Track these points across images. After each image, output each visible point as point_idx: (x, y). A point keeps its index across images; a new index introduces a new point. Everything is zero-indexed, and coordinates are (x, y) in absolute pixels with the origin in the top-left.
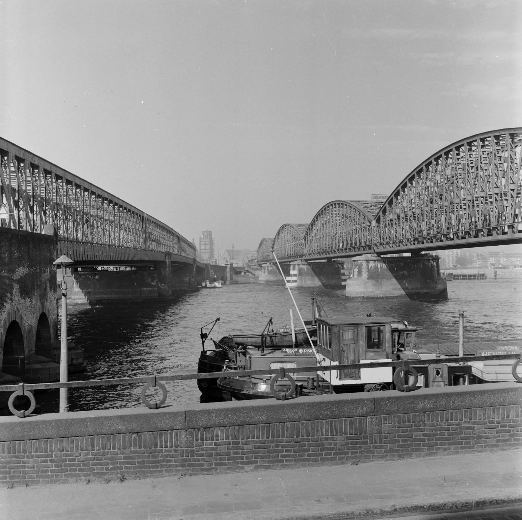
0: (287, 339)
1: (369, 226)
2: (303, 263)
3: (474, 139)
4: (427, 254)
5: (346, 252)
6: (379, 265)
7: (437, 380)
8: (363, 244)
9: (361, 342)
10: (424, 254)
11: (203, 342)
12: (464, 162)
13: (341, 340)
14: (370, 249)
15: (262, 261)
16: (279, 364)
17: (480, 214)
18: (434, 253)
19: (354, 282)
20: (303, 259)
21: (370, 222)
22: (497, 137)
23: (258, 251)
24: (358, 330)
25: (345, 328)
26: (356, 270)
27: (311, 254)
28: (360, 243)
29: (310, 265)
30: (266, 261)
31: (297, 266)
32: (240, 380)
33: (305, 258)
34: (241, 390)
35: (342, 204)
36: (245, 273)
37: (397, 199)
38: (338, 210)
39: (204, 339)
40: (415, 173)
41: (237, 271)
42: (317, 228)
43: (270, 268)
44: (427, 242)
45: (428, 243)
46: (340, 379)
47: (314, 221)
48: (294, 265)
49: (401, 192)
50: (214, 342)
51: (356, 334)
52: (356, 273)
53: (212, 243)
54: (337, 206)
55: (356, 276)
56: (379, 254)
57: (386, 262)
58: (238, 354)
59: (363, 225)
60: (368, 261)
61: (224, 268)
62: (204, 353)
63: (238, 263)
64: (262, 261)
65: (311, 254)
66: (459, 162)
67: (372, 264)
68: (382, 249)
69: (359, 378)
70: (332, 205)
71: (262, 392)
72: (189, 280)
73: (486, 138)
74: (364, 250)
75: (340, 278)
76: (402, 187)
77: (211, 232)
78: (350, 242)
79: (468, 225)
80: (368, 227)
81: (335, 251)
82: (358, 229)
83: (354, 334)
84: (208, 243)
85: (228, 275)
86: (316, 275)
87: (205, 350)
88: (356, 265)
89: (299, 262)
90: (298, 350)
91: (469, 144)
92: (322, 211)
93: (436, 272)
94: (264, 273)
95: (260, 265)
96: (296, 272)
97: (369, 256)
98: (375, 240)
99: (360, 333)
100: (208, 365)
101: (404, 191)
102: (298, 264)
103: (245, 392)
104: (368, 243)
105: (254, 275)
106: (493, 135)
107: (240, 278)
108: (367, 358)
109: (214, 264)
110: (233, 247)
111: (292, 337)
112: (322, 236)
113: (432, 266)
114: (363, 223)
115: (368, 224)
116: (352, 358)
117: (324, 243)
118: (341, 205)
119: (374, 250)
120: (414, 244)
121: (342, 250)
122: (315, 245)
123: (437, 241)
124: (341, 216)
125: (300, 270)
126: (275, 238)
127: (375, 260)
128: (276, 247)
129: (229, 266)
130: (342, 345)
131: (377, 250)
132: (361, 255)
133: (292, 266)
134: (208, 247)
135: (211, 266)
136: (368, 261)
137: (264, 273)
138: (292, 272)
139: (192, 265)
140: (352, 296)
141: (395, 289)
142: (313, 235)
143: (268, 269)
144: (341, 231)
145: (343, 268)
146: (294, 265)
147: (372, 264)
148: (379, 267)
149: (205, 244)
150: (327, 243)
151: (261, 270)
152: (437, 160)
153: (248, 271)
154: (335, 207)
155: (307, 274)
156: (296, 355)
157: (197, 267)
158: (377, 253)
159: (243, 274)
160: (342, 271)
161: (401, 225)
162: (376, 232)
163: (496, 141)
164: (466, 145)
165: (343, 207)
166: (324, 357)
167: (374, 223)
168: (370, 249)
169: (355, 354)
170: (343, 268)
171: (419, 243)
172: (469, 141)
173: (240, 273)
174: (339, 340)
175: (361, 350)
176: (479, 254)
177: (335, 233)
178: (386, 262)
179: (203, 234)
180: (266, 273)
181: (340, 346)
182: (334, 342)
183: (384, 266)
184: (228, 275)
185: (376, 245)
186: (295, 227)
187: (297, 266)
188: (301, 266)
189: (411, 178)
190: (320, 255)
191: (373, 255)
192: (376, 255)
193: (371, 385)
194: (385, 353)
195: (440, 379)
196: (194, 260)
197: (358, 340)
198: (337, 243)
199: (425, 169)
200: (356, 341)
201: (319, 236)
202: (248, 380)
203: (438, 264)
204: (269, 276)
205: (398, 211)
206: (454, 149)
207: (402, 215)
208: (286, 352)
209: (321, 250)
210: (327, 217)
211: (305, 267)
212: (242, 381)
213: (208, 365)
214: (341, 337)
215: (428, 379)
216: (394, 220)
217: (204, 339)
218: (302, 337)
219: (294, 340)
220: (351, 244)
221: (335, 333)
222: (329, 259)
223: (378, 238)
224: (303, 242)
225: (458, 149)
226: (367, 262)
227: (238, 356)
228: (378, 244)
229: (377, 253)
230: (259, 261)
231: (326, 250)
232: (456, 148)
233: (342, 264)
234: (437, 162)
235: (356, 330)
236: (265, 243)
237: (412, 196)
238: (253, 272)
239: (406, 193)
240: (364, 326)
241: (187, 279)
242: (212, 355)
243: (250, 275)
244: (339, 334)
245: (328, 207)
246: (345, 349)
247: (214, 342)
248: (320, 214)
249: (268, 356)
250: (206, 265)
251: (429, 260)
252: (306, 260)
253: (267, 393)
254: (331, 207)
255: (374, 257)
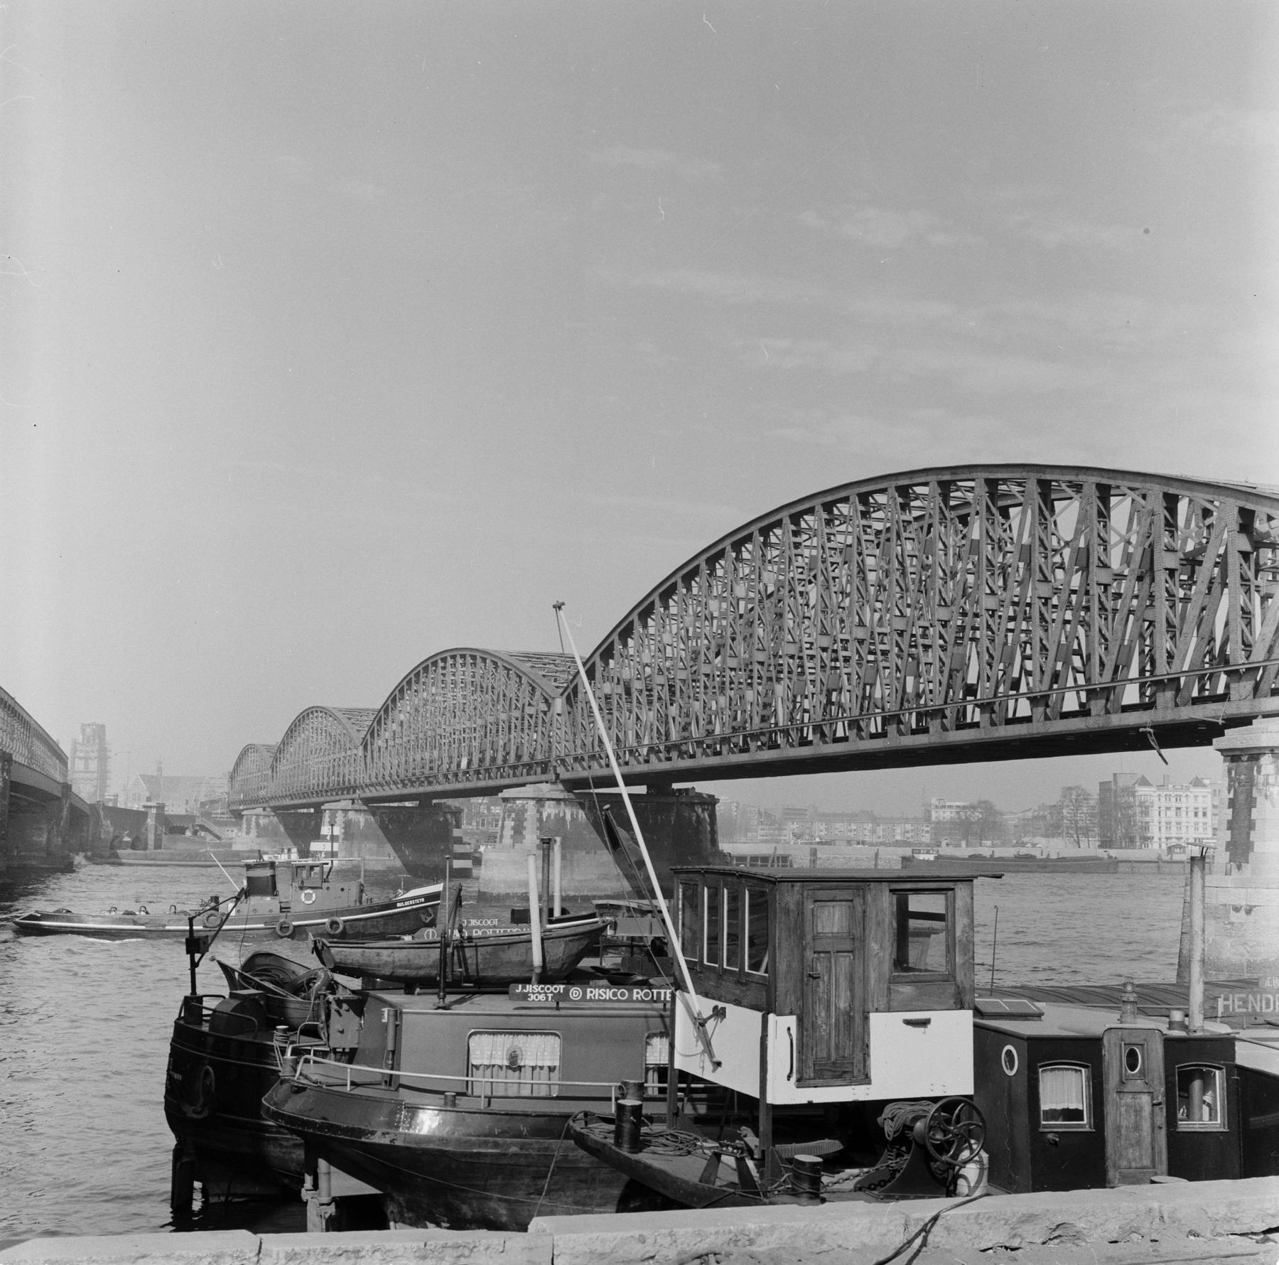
0: (513, 955)
1: (545, 713)
2: (356, 807)
3: (842, 494)
4: (687, 790)
5: (478, 779)
6: (568, 812)
7: (1130, 1087)
8: (526, 759)
9: (874, 946)
10: (679, 790)
11: (194, 965)
12: (814, 552)
13: (809, 937)
14: (544, 771)
15: (241, 802)
16: (500, 1038)
17: (854, 682)
18: (703, 787)
19: (503, 856)
20: (356, 796)
21: (546, 701)
22: (904, 491)
23: (232, 778)
24: (865, 903)
25: (822, 894)
26: (509, 824)
27: (372, 785)
28: (519, 757)
29: (374, 815)
30: (252, 802)
31: (340, 815)
32: (360, 1097)
33: (363, 795)
34: (362, 1133)
35: (474, 657)
36: (195, 833)
37: (625, 645)
38: (463, 673)
39: (197, 956)
40: (678, 578)
41: (173, 827)
42: (402, 717)
43: (262, 821)
44: (705, 753)
45: (708, 756)
46: (801, 1082)
47: (394, 701)
48: (334, 812)
49: (638, 629)
50: (224, 967)
51: (859, 914)
52: (508, 832)
53: (103, 757)
54: (460, 661)
55: (507, 840)
56: (571, 785)
57: (587, 804)
58: (334, 1006)
59: (529, 710)
60: (540, 801)
61: (140, 816)
62: (192, 1004)
63: (175, 808)
64: (241, 802)
65: (372, 785)
66: (799, 551)
67: (550, 810)
68: (580, 772)
69: (866, 1079)
70: (444, 660)
71: (428, 1139)
72: (49, 839)
73: (323, 803)
74: (528, 774)
75: (449, 851)
76: (640, 615)
77: (103, 726)
78: (489, 753)
79: (820, 711)
80: (541, 715)
81: (446, 776)
82: (513, 720)
83: (852, 917)
84: (95, 754)
85: (151, 837)
86: (390, 841)
87: (200, 992)
88: (510, 812)
89: (346, 804)
90: (567, 991)
91: (828, 507)
92: (417, 675)
93: (709, 836)
94: (248, 833)
95: (238, 815)
96: (337, 831)
97: (546, 789)
98: (559, 749)
99: (872, 913)
100: (210, 1040)
101: (645, 626)
102: (345, 811)
103: (377, 1139)
104: (539, 757)
105: (219, 838)
106: (893, 484)
107: (181, 845)
108: (894, 1004)
109: (110, 805)
110: (160, 769)
111: (529, 951)
112: (413, 737)
113: (700, 821)
114: (530, 705)
115: (544, 707)
116: (843, 1005)
117: (418, 757)
118: (469, 660)
119: (557, 775)
120: (669, 759)
121: (466, 773)
122: (391, 763)
123: (731, 751)
124: (469, 686)
125: (348, 825)
126: (283, 742)
127: (558, 800)
128: (283, 767)
129: (154, 811)
130: (809, 954)
131: (564, 775)
132: (523, 785)
133: (327, 814)
134: (93, 765)
135: (106, 808)
136: (540, 801)
137: (248, 833)
138: (325, 830)
139: (58, 799)
140: (495, 892)
141: (605, 877)
142: (388, 735)
143: (258, 825)
144: (468, 724)
145: (458, 826)
146: (334, 812)
147: (550, 810)
148: (568, 817)
149: (87, 759)
150: (427, 755)
151: (239, 825)
152: (737, 546)
153: (203, 828)
154: (454, 665)
155: (365, 836)
156: (558, 1008)
157: (73, 808)
158: (564, 782)
159: (188, 833)
160: (456, 833)
161: (635, 710)
162: (564, 729)
163: (900, 500)
164: (819, 509)
165: (474, 664)
166: (715, 1003)
167: (559, 705)
168: (544, 771)
169: (852, 990)
170: (458, 826)
171: (681, 755)
172: (829, 498)
173: (182, 831)
174: (802, 937)
175: (873, 976)
176: (762, 810)
177: (449, 730)
178: (587, 804)
179: (83, 731)
180: (253, 833)
181: (802, 958)
182: (785, 944)
183: (582, 815)
184: (151, 837)
185: (563, 761)
186: (339, 715)
187: (340, 815)
188: (351, 815)
189: (666, 591)
190: (405, 786)
191: (554, 787)
192: (561, 787)
193: (908, 1107)
194: (951, 989)
195: (1139, 1084)
196: (67, 788)
197: (863, 940)
198: (455, 755)
199: (705, 570)
200: (856, 942)
201: (405, 739)
202: (387, 1095)
203: (713, 816)
204: (259, 840)
205: (627, 674)
206: (787, 521)
207: (637, 685)
208: (525, 997)
209: (410, 775)
210: (429, 690)
211: (361, 819)
212: (368, 1099)
213: (210, 1040)
214: (808, 928)
215: (1101, 1084)
216: (615, 698)
217: (197, 956)
218: (562, 949)
219: (537, 959)
220: (493, 759)
221: (787, 912)
222: (424, 799)
223: (570, 745)
224: (360, 752)
225: (795, 519)
226: (539, 802)
227: (334, 1015)
228: (570, 760)
229: (564, 782)
230: (234, 803)
231: (414, 775)
232: (791, 516)
233: (457, 813)
234: (739, 552)
235: (858, 901)
236: (252, 756)
237: (667, 638)
238: (216, 829)
239: (652, 630)
240: (885, 887)
241: (44, 839)
242: (228, 1009)
243: (209, 837)
244: (801, 913)
245: (435, 664)
246: (820, 968)
247: (224, 967)
248: (409, 683)
249: (457, 1009)
250: (92, 806)
251: (692, 805)
252: (367, 801)
253: (442, 1140)
254: (441, 664)
255: (558, 792)
